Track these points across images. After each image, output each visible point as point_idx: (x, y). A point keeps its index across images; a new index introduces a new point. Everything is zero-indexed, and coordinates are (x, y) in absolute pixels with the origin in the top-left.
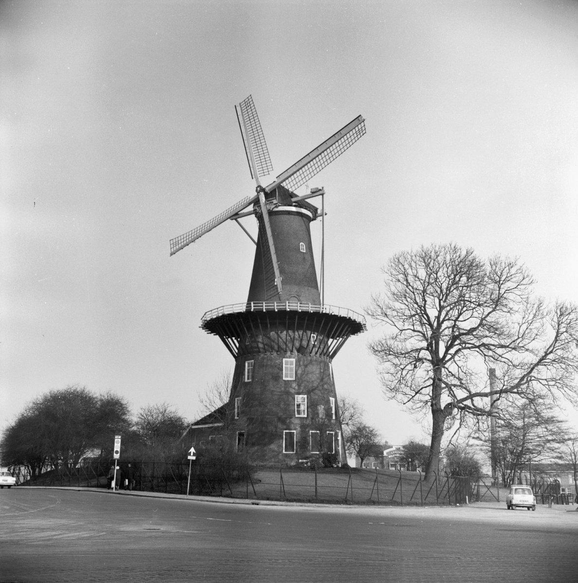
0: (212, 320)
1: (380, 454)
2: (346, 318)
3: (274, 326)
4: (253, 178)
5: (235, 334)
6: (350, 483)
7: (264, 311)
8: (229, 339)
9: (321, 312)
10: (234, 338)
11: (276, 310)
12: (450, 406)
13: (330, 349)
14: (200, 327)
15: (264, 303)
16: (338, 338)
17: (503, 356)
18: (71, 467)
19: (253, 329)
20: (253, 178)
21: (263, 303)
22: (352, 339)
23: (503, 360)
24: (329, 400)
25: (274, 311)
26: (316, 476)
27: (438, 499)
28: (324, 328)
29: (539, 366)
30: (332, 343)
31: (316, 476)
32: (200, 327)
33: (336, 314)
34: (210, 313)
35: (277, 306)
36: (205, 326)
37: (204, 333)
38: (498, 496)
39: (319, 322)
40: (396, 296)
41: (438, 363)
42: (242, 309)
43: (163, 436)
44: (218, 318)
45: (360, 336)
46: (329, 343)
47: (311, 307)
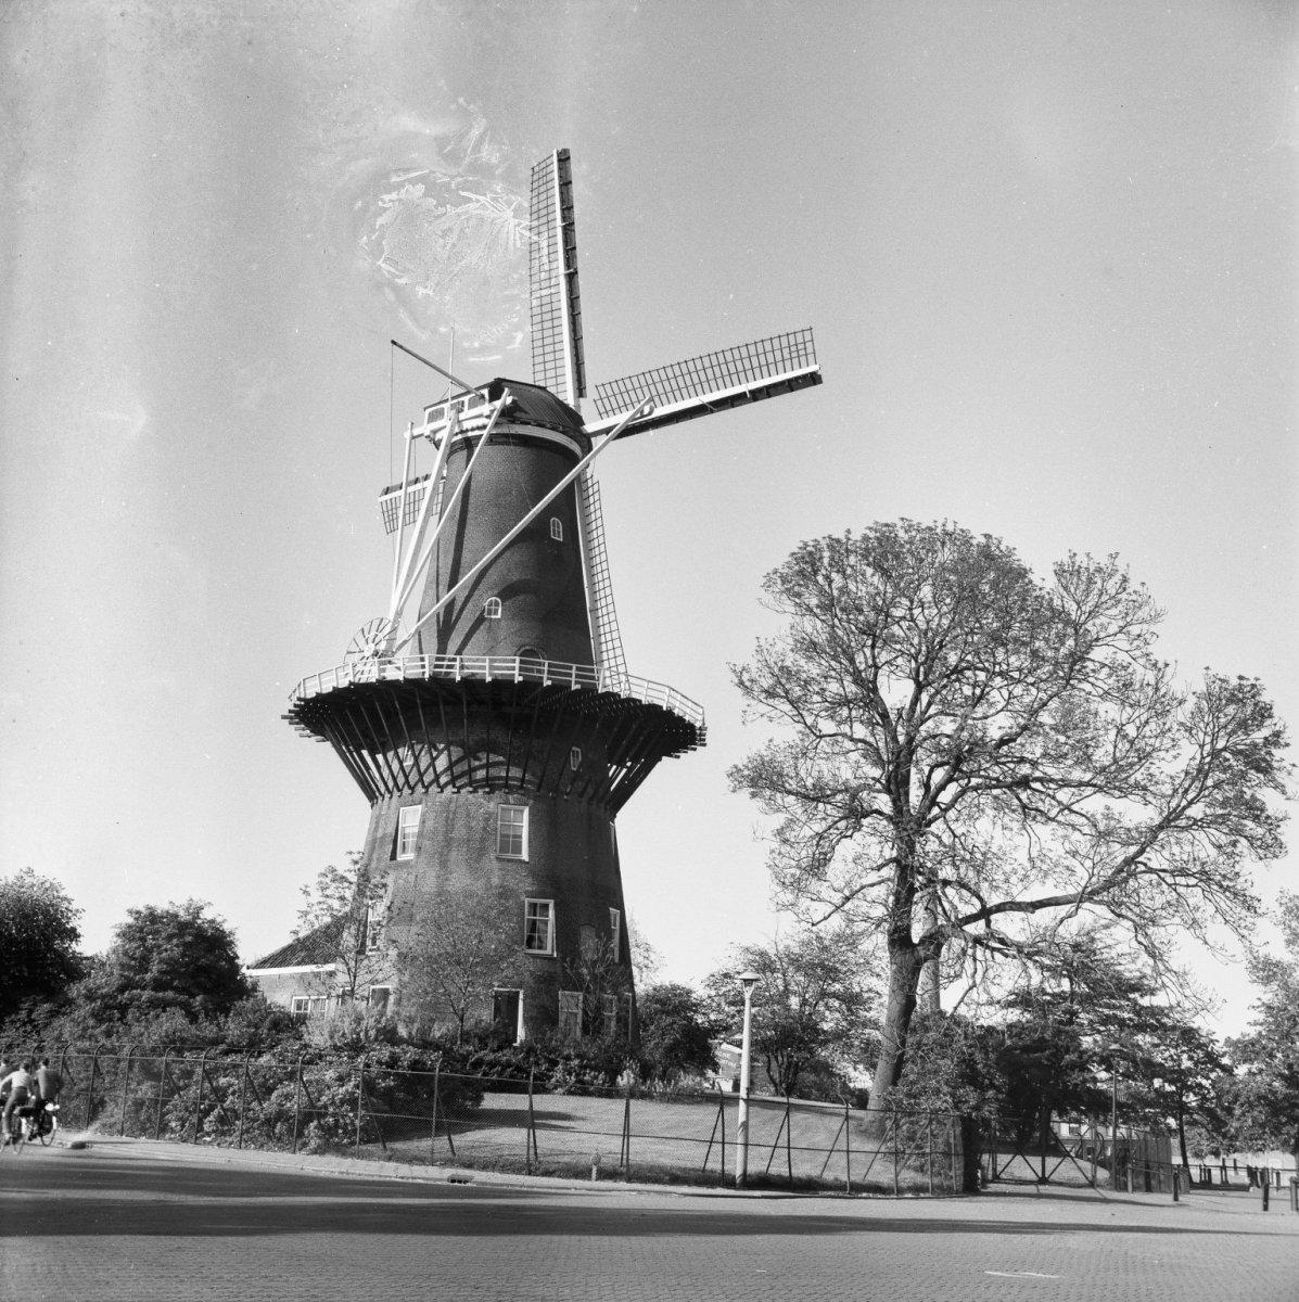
0: (320, 698)
4: (813, 379)
6: (786, 1124)
10: (365, 753)
11: (489, 679)
12: (935, 940)
14: (284, 717)
15: (574, 668)
17: (1075, 807)
20: (813, 379)
21: (571, 668)
23: (1074, 818)
24: (609, 914)
26: (450, 1139)
28: (394, 726)
31: (450, 1139)
32: (284, 717)
36: (297, 714)
39: (409, 707)
40: (811, 648)
41: (909, 826)
43: (970, 951)
44: (337, 693)
47: (484, 668)
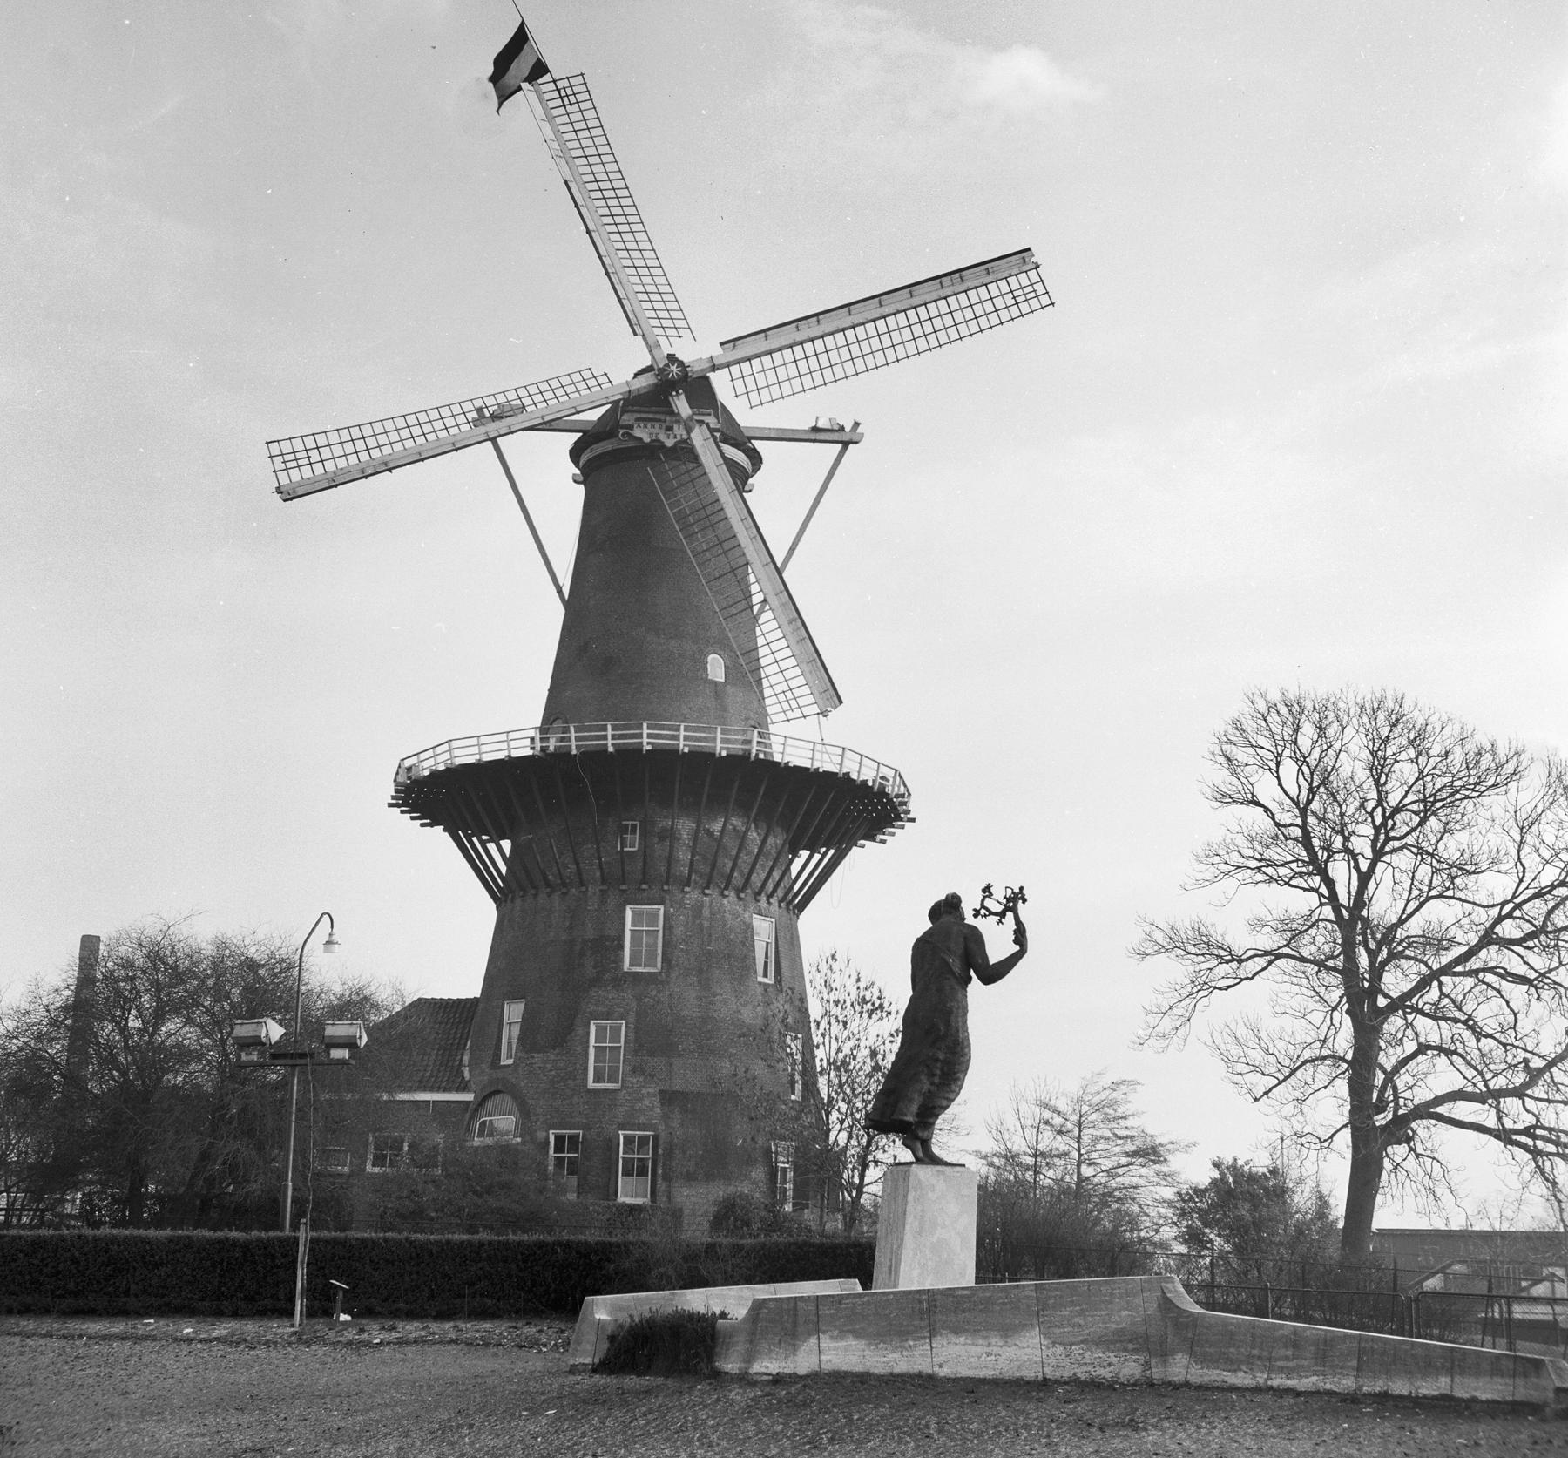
1: (557, 1418)
2: (836, 774)
3: (718, 803)
5: (489, 826)
7: (611, 749)
8: (492, 847)
9: (752, 758)
13: (796, 888)
16: (823, 850)
18: (230, 1184)
19: (731, 805)
22: (863, 858)
25: (569, 753)
27: (1464, 1009)
29: (774, 1372)
30: (802, 863)
33: (806, 764)
34: (430, 753)
35: (649, 736)
37: (406, 825)
38: (1441, 1118)
42: (522, 750)
45: (898, 839)
46: (795, 868)
47: (686, 738)
